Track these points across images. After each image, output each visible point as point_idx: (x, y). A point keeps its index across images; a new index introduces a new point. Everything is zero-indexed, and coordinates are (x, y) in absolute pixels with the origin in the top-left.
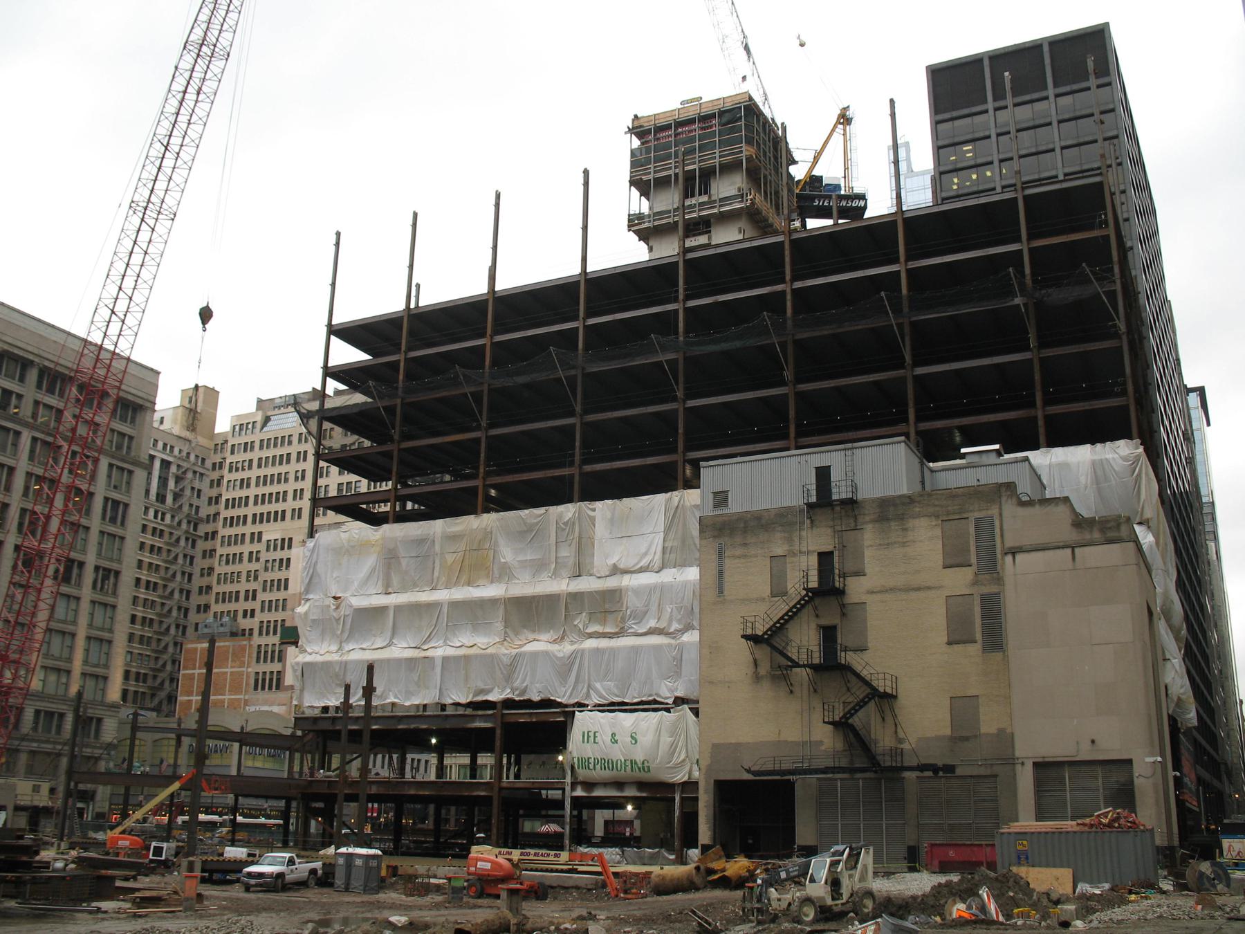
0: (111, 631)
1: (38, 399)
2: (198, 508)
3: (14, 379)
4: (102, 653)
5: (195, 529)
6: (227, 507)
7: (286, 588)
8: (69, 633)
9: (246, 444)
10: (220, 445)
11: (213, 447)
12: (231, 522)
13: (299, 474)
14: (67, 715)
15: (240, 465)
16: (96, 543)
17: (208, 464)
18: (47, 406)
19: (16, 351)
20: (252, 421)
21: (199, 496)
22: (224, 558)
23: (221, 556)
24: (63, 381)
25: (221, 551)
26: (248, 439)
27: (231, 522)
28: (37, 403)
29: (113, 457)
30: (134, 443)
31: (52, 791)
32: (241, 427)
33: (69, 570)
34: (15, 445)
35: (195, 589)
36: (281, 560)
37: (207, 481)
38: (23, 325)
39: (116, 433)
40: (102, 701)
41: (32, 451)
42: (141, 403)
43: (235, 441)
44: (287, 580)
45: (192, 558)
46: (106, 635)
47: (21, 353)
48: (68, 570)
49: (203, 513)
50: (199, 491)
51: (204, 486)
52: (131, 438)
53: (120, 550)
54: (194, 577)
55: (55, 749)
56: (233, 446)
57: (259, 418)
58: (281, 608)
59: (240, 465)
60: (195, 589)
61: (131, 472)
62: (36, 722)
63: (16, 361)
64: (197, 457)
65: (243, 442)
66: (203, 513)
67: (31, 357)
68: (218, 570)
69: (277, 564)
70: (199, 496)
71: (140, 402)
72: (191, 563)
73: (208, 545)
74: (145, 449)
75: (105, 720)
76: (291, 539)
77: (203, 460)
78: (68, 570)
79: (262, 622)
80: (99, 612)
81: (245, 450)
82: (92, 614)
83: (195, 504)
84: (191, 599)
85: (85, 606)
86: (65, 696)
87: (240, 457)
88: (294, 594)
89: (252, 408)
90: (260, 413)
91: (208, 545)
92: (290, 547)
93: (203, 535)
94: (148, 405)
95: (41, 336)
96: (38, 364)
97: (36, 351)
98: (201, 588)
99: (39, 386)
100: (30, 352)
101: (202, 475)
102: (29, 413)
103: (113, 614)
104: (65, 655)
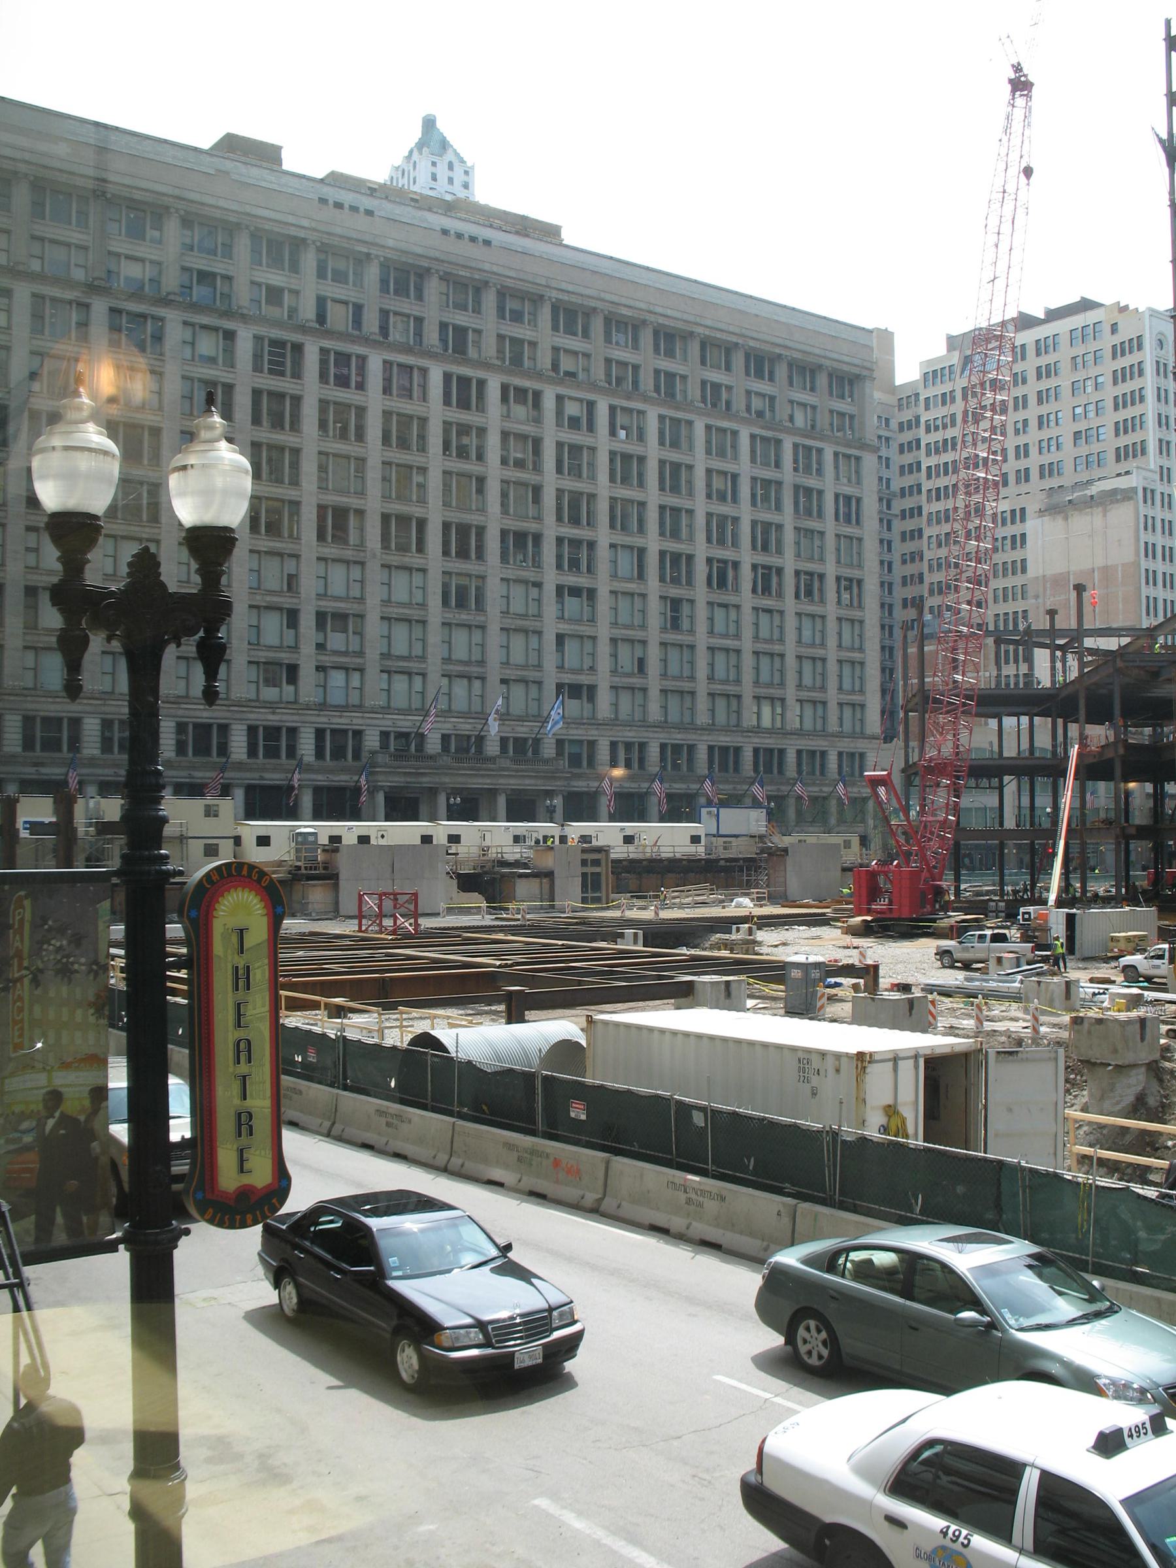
0: (861, 649)
1: (557, 345)
2: (888, 480)
3: (720, 368)
4: (585, 656)
5: (889, 508)
6: (929, 477)
7: (1024, 570)
8: (639, 641)
9: (944, 395)
10: (908, 398)
11: (896, 403)
12: (938, 494)
13: (1020, 425)
14: (651, 744)
15: (939, 422)
16: (833, 550)
17: (894, 424)
18: (758, 394)
19: (719, 335)
20: (947, 365)
21: (888, 467)
22: (934, 539)
23: (930, 537)
24: (851, 383)
25: (929, 532)
26: (946, 388)
27: (938, 494)
28: (556, 350)
29: (837, 444)
30: (856, 421)
31: (864, 841)
32: (932, 375)
33: (809, 585)
34: (734, 447)
35: (897, 578)
36: (1014, 537)
37: (895, 446)
38: (719, 302)
39: (147, 264)
40: (737, 726)
41: (753, 452)
42: (593, 305)
43: (931, 392)
44: (1024, 561)
45: (889, 543)
46: (856, 656)
47: (724, 336)
48: (766, 579)
49: (896, 486)
50: (887, 459)
51: (892, 452)
52: (852, 417)
53: (859, 554)
54: (894, 566)
55: (821, 791)
56: (927, 399)
57: (955, 359)
58: (1020, 596)
59: (939, 422)
60: (898, 580)
61: (858, 459)
62: (663, 758)
63: (719, 347)
64: (879, 417)
65: (939, 393)
66: (896, 486)
67: (734, 339)
68: (927, 555)
69: (1008, 542)
70: (888, 467)
71: (856, 371)
72: (889, 550)
73: (910, 525)
74: (871, 428)
75: (234, 727)
76: (1023, 510)
77: (887, 420)
78: (766, 579)
79: (997, 615)
80: (623, 604)
81: (944, 403)
82: (756, 625)
83: (885, 476)
84: (894, 593)
85: (832, 625)
86: (692, 723)
87: (938, 412)
88: (1037, 578)
89: (941, 350)
90: (956, 354)
91: (910, 525)
92: (1023, 520)
93: (898, 512)
94: (865, 373)
95: (740, 311)
96: (377, 256)
97: (737, 330)
98: (904, 578)
99: (555, 328)
100: (733, 333)
101: (887, 439)
102: (743, 407)
103: (782, 621)
104: (533, 660)
